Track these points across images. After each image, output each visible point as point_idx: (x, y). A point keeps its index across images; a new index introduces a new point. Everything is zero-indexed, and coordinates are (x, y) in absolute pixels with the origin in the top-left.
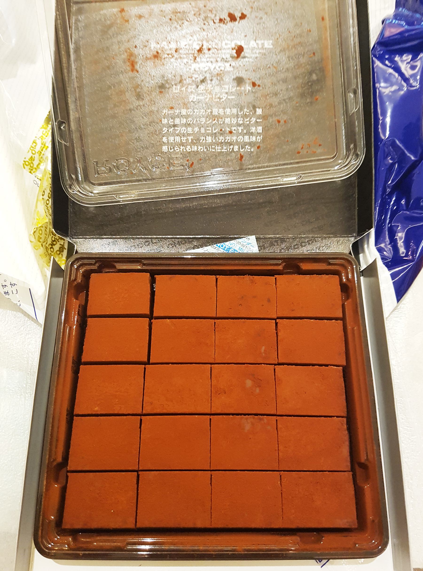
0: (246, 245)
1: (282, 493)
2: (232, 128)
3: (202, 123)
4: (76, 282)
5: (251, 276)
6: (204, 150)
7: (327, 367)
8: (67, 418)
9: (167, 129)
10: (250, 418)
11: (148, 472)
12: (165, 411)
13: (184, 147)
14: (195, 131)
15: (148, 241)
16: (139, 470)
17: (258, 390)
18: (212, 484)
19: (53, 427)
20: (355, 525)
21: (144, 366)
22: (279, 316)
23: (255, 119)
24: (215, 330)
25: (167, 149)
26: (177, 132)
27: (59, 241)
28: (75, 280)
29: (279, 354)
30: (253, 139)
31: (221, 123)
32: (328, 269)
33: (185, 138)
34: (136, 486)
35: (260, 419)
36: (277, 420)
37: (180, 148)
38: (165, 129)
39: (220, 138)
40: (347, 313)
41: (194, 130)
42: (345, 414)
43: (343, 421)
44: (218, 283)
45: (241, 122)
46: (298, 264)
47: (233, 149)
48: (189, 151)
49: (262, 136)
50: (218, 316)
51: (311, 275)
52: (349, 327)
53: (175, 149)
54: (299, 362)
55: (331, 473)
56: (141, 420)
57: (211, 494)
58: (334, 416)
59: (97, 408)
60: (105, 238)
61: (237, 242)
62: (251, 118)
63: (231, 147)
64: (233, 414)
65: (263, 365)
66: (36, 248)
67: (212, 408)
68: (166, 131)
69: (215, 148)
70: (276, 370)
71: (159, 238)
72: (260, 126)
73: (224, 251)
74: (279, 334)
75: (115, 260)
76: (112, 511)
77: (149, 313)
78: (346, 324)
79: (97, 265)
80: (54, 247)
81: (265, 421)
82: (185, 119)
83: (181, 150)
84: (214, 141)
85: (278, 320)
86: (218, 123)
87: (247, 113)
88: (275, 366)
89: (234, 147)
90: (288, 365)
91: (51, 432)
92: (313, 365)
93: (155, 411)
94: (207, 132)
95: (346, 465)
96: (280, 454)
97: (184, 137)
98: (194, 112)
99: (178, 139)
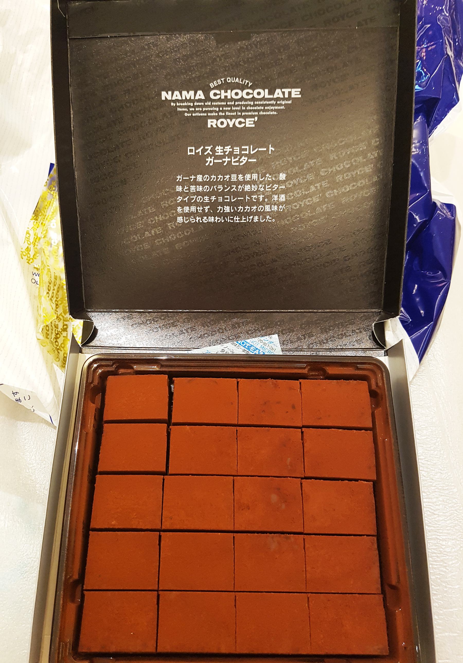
0: (268, 344)
1: (309, 617)
4: (93, 384)
5: (274, 380)
7: (357, 482)
8: (83, 531)
10: (276, 536)
12: (185, 527)
16: (159, 589)
17: (284, 506)
18: (237, 606)
19: (69, 541)
20: (386, 652)
21: (163, 476)
22: (305, 424)
24: (237, 439)
27: (62, 334)
28: (92, 383)
29: (306, 467)
32: (356, 373)
34: (156, 606)
35: (287, 538)
36: (304, 539)
37: (196, 219)
41: (211, 199)
42: (376, 534)
43: (374, 540)
44: (239, 387)
47: (253, 219)
48: (206, 222)
50: (240, 423)
51: (339, 381)
52: (380, 439)
53: (191, 220)
54: (327, 476)
55: (361, 595)
56: (160, 536)
58: (364, 535)
59: (114, 522)
61: (259, 340)
63: (251, 217)
65: (289, 478)
66: (44, 345)
67: (235, 525)
70: (303, 485)
73: (245, 348)
74: (305, 445)
76: (132, 633)
77: (167, 418)
78: (376, 434)
79: (114, 366)
80: (58, 340)
81: (292, 539)
83: (197, 221)
85: (303, 429)
88: (302, 480)
89: (253, 217)
90: (316, 479)
91: (67, 547)
92: (343, 480)
93: (175, 527)
95: (376, 587)
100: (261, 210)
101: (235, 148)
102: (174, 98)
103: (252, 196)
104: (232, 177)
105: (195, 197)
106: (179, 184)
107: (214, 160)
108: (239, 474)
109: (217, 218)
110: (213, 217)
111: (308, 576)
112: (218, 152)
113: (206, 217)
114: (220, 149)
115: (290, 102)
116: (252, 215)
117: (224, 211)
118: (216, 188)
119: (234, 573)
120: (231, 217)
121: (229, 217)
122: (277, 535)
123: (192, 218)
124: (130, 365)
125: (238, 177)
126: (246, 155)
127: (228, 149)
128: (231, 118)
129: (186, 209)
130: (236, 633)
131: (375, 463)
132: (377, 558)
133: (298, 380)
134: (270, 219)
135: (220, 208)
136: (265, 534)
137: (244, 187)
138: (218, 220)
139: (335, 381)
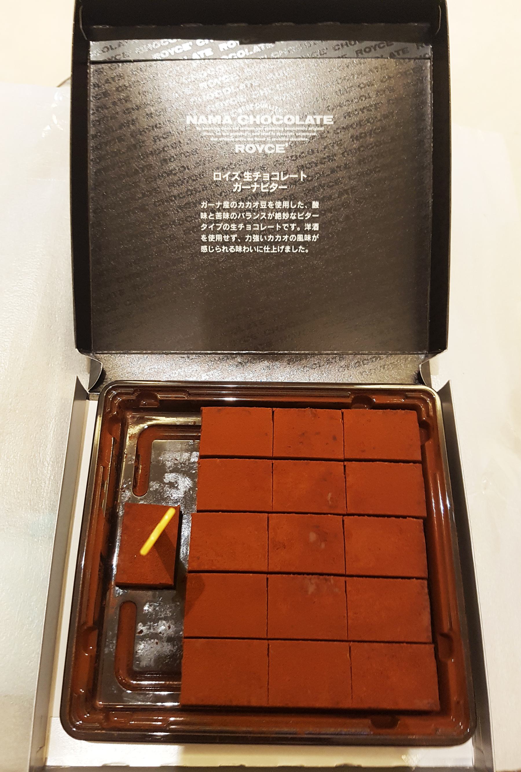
2: (283, 225)
3: (248, 219)
5: (313, 409)
6: (249, 251)
8: (99, 575)
9: (206, 225)
10: (315, 578)
11: (194, 640)
12: (214, 568)
13: (226, 248)
14: (240, 228)
15: (184, 358)
17: (323, 546)
20: (437, 707)
23: (310, 214)
24: (272, 473)
25: (206, 249)
26: (218, 229)
30: (308, 238)
31: (271, 218)
33: (228, 237)
35: (326, 580)
36: (345, 582)
37: (222, 249)
38: (204, 225)
39: (269, 237)
40: (427, 455)
41: (239, 227)
42: (425, 575)
45: (294, 218)
46: (370, 396)
47: (284, 249)
48: (232, 252)
49: (318, 235)
53: (216, 249)
57: (269, 667)
60: (134, 353)
62: (305, 213)
63: (282, 247)
64: (294, 573)
68: (205, 228)
69: (262, 249)
71: (196, 354)
72: (317, 222)
75: (157, 389)
82: (228, 214)
83: (223, 250)
84: (262, 240)
86: (267, 218)
87: (301, 207)
89: (285, 247)
92: (389, 516)
94: (254, 229)
95: (426, 635)
96: (350, 622)
97: (226, 235)
98: (239, 205)
99: (219, 237)
100: (294, 239)
101: (264, 174)
102: (200, 122)
103: (283, 225)
104: (261, 204)
105: (221, 225)
106: (204, 210)
107: (242, 185)
108: (274, 510)
109: (245, 248)
110: (240, 247)
111: (350, 622)
112: (246, 178)
113: (233, 247)
114: (248, 175)
115: (322, 129)
116: (283, 245)
117: (253, 239)
118: (245, 215)
119: (267, 618)
120: (260, 247)
121: (258, 247)
122: (316, 576)
123: (217, 248)
124: (154, 394)
125: (267, 204)
126: (275, 182)
127: (257, 175)
128: (260, 143)
129: (211, 238)
130: (268, 684)
131: (425, 498)
132: (428, 604)
133: (340, 409)
134: (303, 250)
135: (248, 236)
136: (302, 576)
137: (275, 215)
138: (247, 250)
139: (381, 410)
